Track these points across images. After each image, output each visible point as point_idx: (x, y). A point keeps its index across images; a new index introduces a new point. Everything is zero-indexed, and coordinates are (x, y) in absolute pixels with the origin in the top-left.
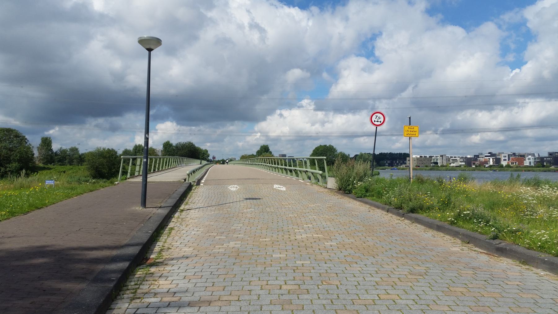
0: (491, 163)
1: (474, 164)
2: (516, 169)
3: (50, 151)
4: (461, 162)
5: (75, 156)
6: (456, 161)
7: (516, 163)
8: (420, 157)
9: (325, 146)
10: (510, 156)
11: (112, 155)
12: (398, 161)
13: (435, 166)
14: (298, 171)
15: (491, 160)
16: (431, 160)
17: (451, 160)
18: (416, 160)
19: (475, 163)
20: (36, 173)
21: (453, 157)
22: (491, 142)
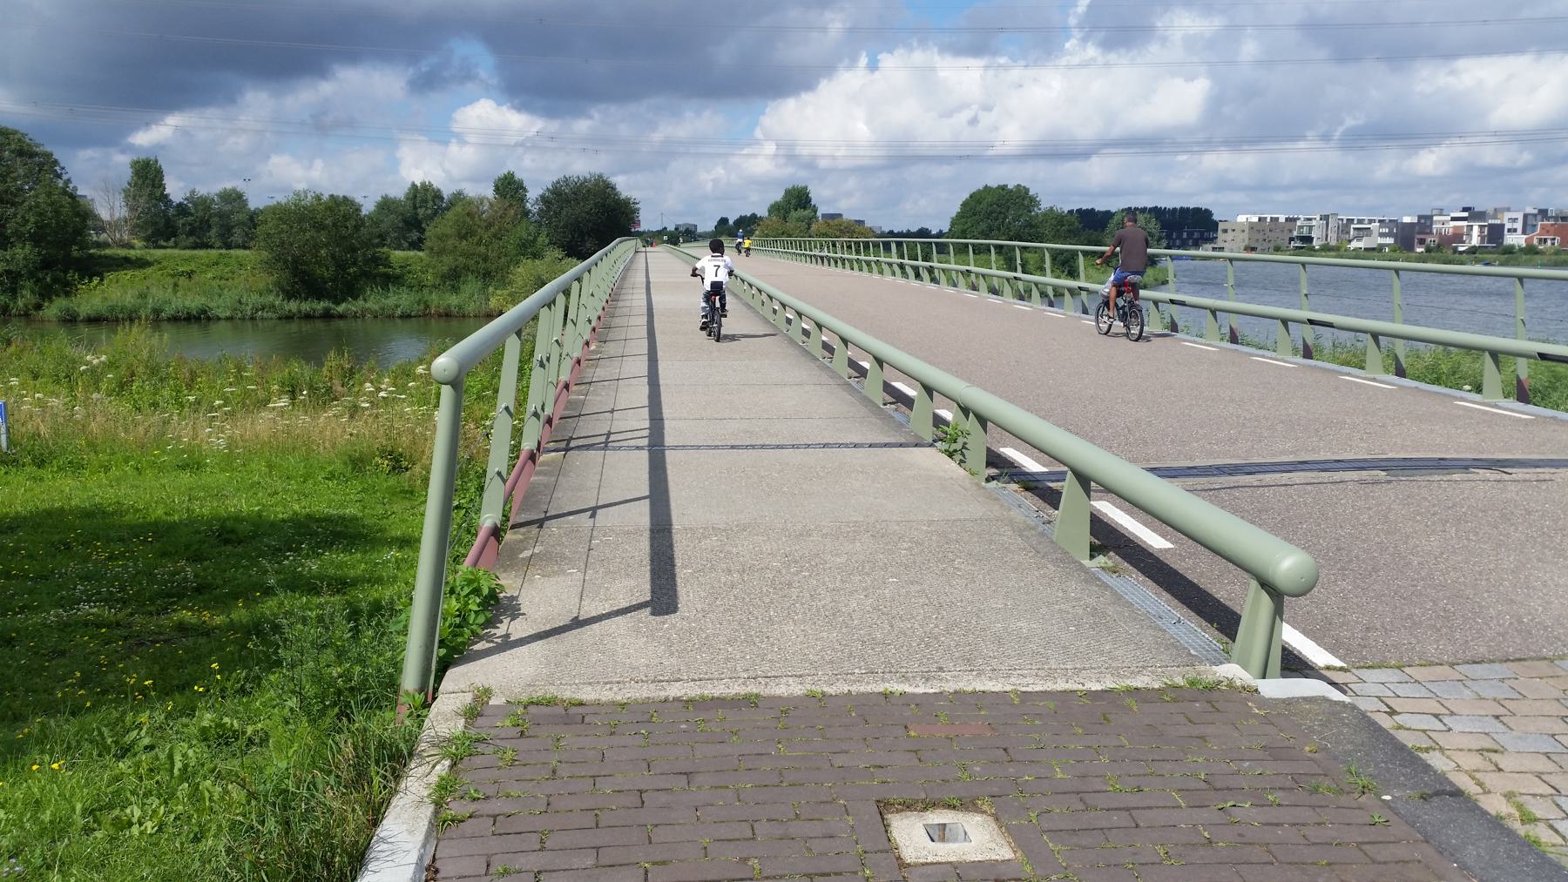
0: (1475, 240)
1: (1422, 242)
2: (1554, 257)
3: (160, 200)
4: (1382, 235)
5: (236, 218)
6: (1363, 232)
7: (1554, 239)
8: (1260, 219)
9: (1003, 189)
10: (1529, 217)
11: (346, 218)
12: (1185, 234)
13: (1302, 248)
14: (873, 263)
15: (1476, 230)
16: (1291, 231)
17: (1352, 230)
18: (1247, 231)
19: (1425, 240)
20: (96, 280)
21: (1355, 222)
22: (1473, 173)
